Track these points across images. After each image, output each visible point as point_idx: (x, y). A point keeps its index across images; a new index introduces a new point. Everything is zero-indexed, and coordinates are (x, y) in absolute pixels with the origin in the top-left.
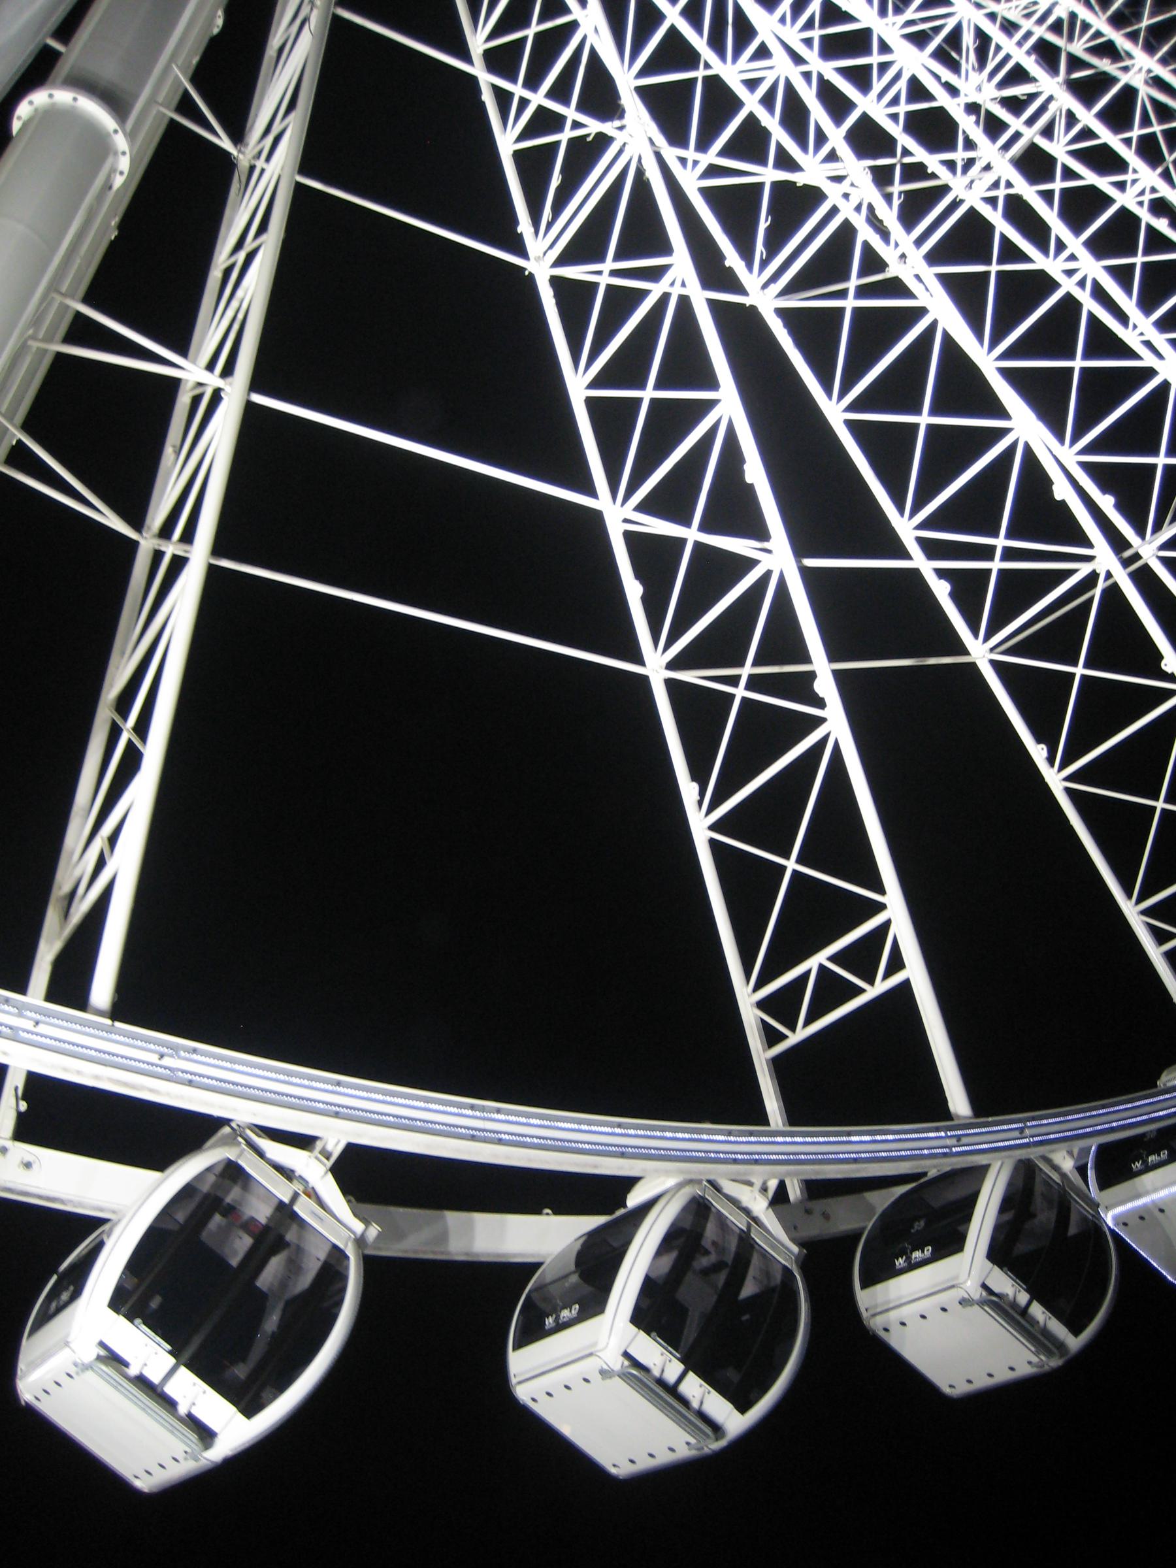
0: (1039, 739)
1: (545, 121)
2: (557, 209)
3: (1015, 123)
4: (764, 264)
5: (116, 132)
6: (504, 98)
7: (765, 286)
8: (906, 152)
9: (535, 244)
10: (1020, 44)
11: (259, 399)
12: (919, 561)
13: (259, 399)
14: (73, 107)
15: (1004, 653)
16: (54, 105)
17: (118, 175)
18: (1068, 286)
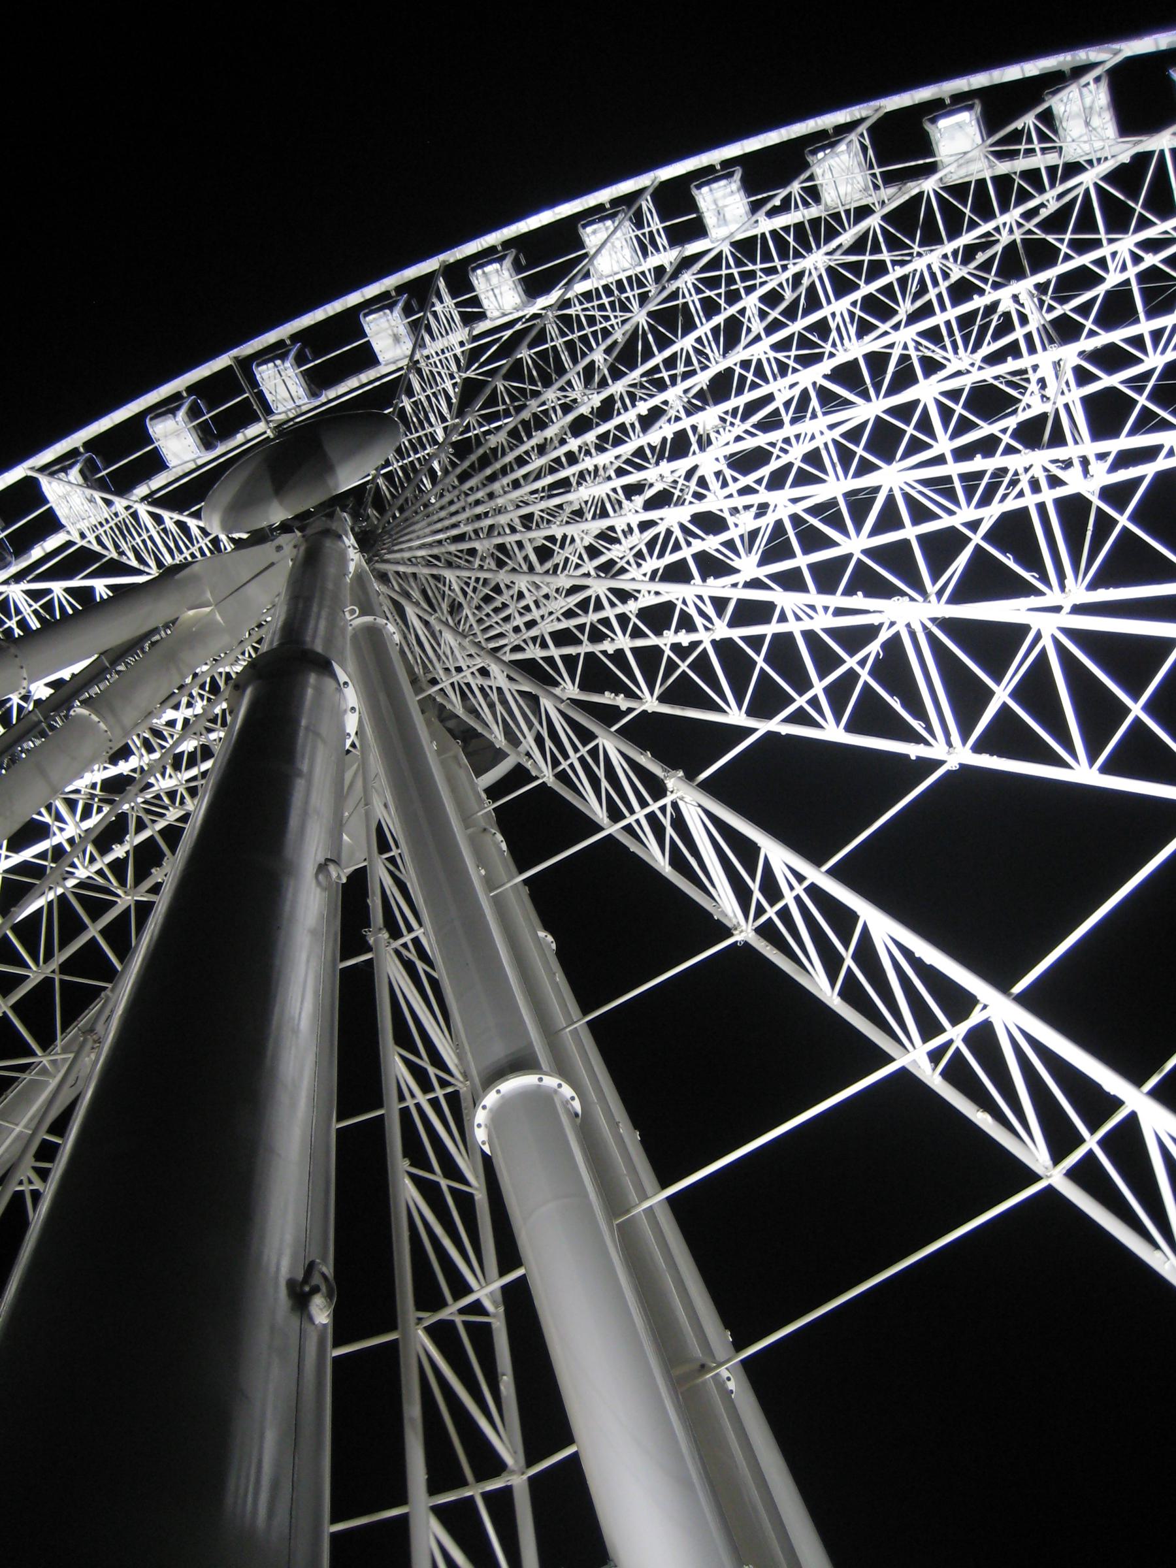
0: (1028, 569)
1: (838, 694)
2: (921, 714)
3: (1019, 333)
4: (1045, 579)
5: (541, 1080)
6: (800, 718)
7: (1062, 587)
8: (1004, 431)
9: (936, 750)
10: (943, 308)
11: (1018, 988)
12: (763, 727)
13: (1018, 988)
14: (503, 1097)
15: (63, 945)
16: (491, 1110)
17: (572, 1102)
18: (1018, 236)
